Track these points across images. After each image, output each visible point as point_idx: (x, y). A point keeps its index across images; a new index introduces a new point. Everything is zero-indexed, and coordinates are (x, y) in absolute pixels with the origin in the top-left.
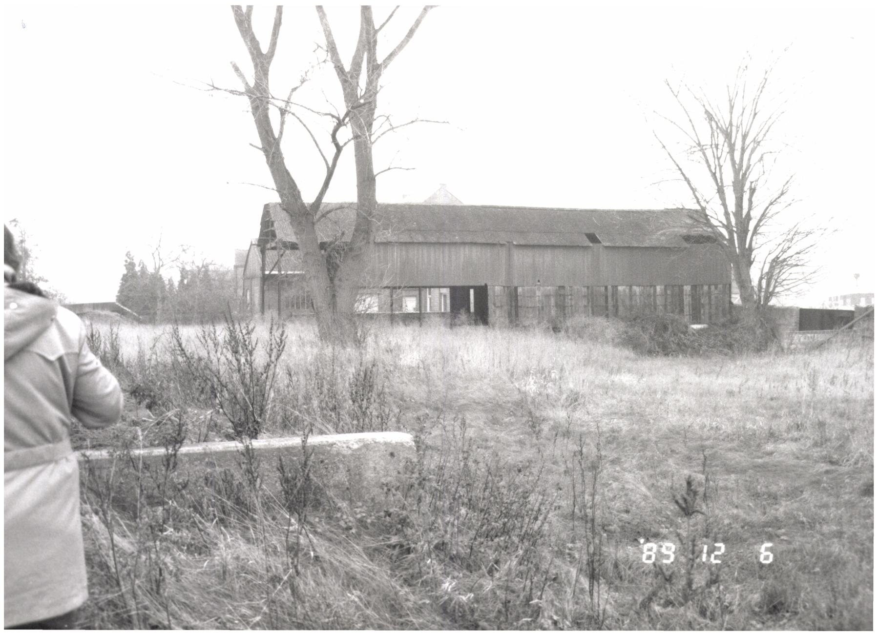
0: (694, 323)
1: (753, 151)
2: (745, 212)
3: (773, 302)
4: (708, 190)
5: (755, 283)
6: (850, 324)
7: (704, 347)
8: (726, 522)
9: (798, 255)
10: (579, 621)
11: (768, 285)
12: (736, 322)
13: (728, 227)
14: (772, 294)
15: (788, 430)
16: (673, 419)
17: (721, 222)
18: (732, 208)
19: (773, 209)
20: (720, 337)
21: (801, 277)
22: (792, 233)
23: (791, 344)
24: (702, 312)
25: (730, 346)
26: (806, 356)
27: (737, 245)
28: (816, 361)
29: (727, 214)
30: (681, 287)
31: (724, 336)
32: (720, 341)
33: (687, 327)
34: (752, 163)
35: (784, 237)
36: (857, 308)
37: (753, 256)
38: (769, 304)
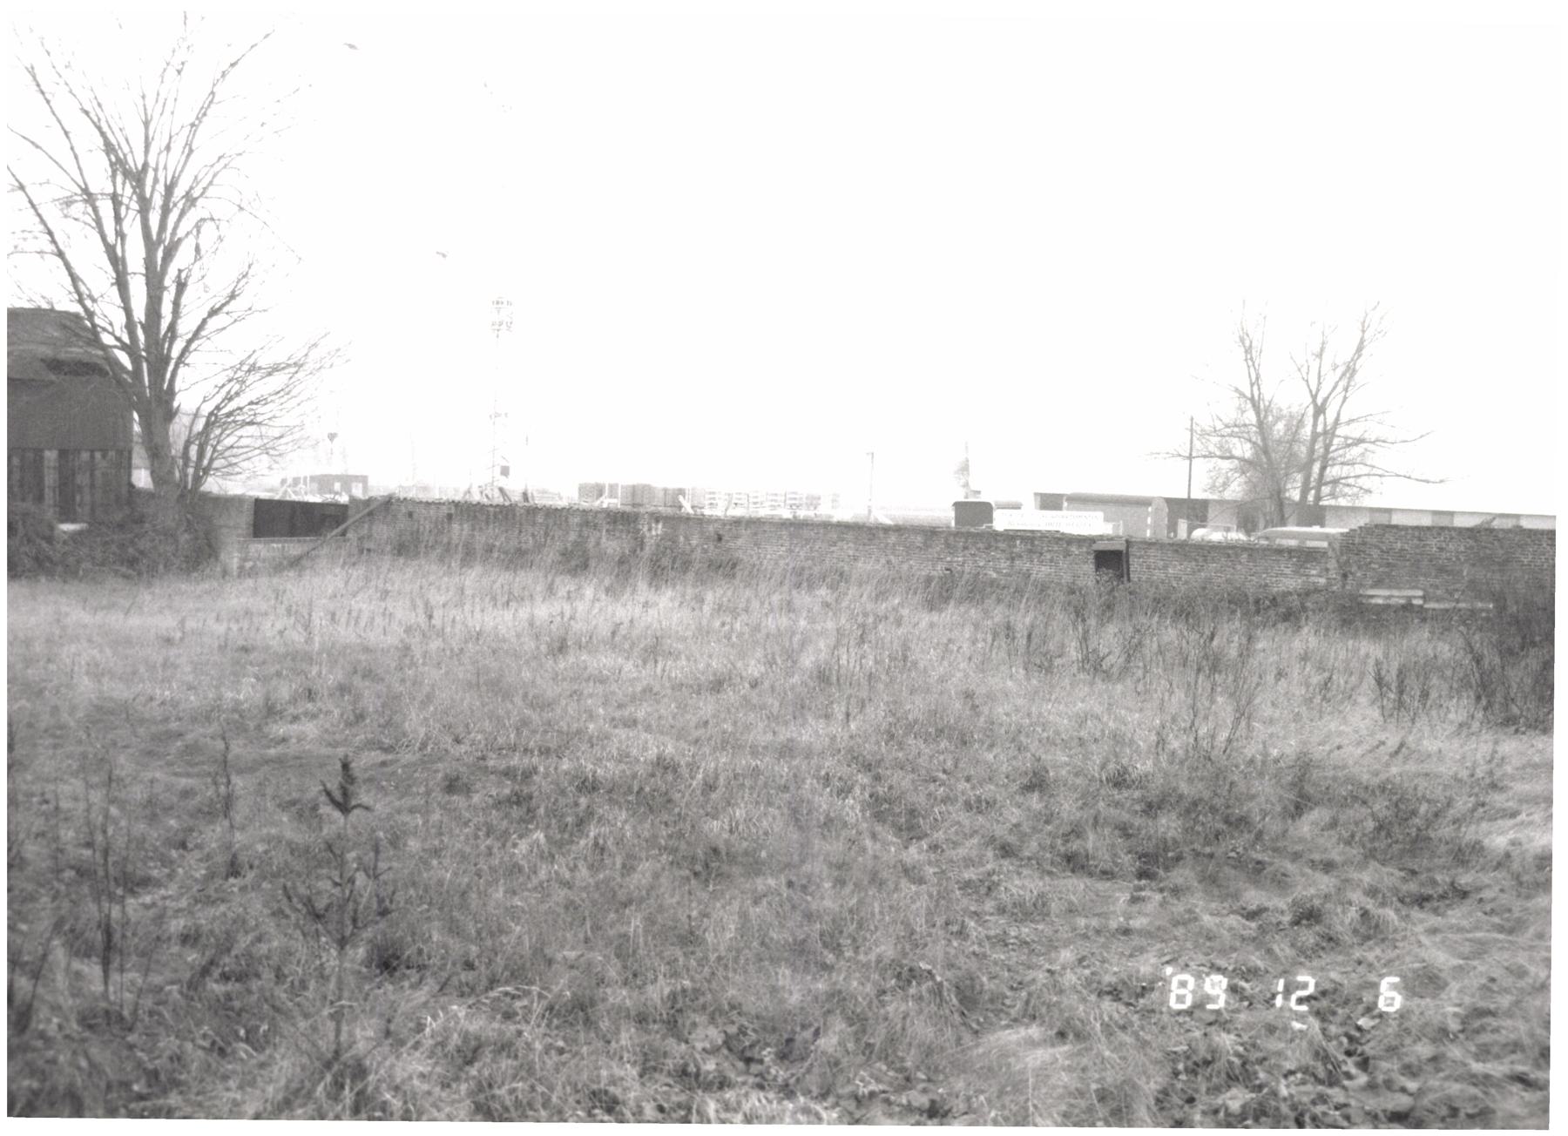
0: (63, 522)
1: (182, 214)
2: (164, 325)
3: (212, 485)
4: (99, 278)
5: (176, 449)
6: (343, 526)
7: (86, 565)
8: (260, 848)
9: (254, 407)
10: (93, 1022)
11: (201, 454)
12: (140, 521)
13: (131, 349)
14: (206, 471)
15: (294, 701)
16: (85, 687)
17: (118, 339)
18: (139, 314)
19: (213, 323)
20: (114, 548)
21: (259, 443)
22: (245, 368)
23: (245, 560)
24: (78, 498)
25: (132, 562)
26: (275, 580)
27: (147, 383)
28: (297, 588)
29: (130, 326)
30: (39, 452)
31: (122, 546)
32: (114, 554)
33: (52, 528)
34: (180, 233)
35: (230, 373)
36: (353, 500)
37: (175, 404)
38: (202, 489)
